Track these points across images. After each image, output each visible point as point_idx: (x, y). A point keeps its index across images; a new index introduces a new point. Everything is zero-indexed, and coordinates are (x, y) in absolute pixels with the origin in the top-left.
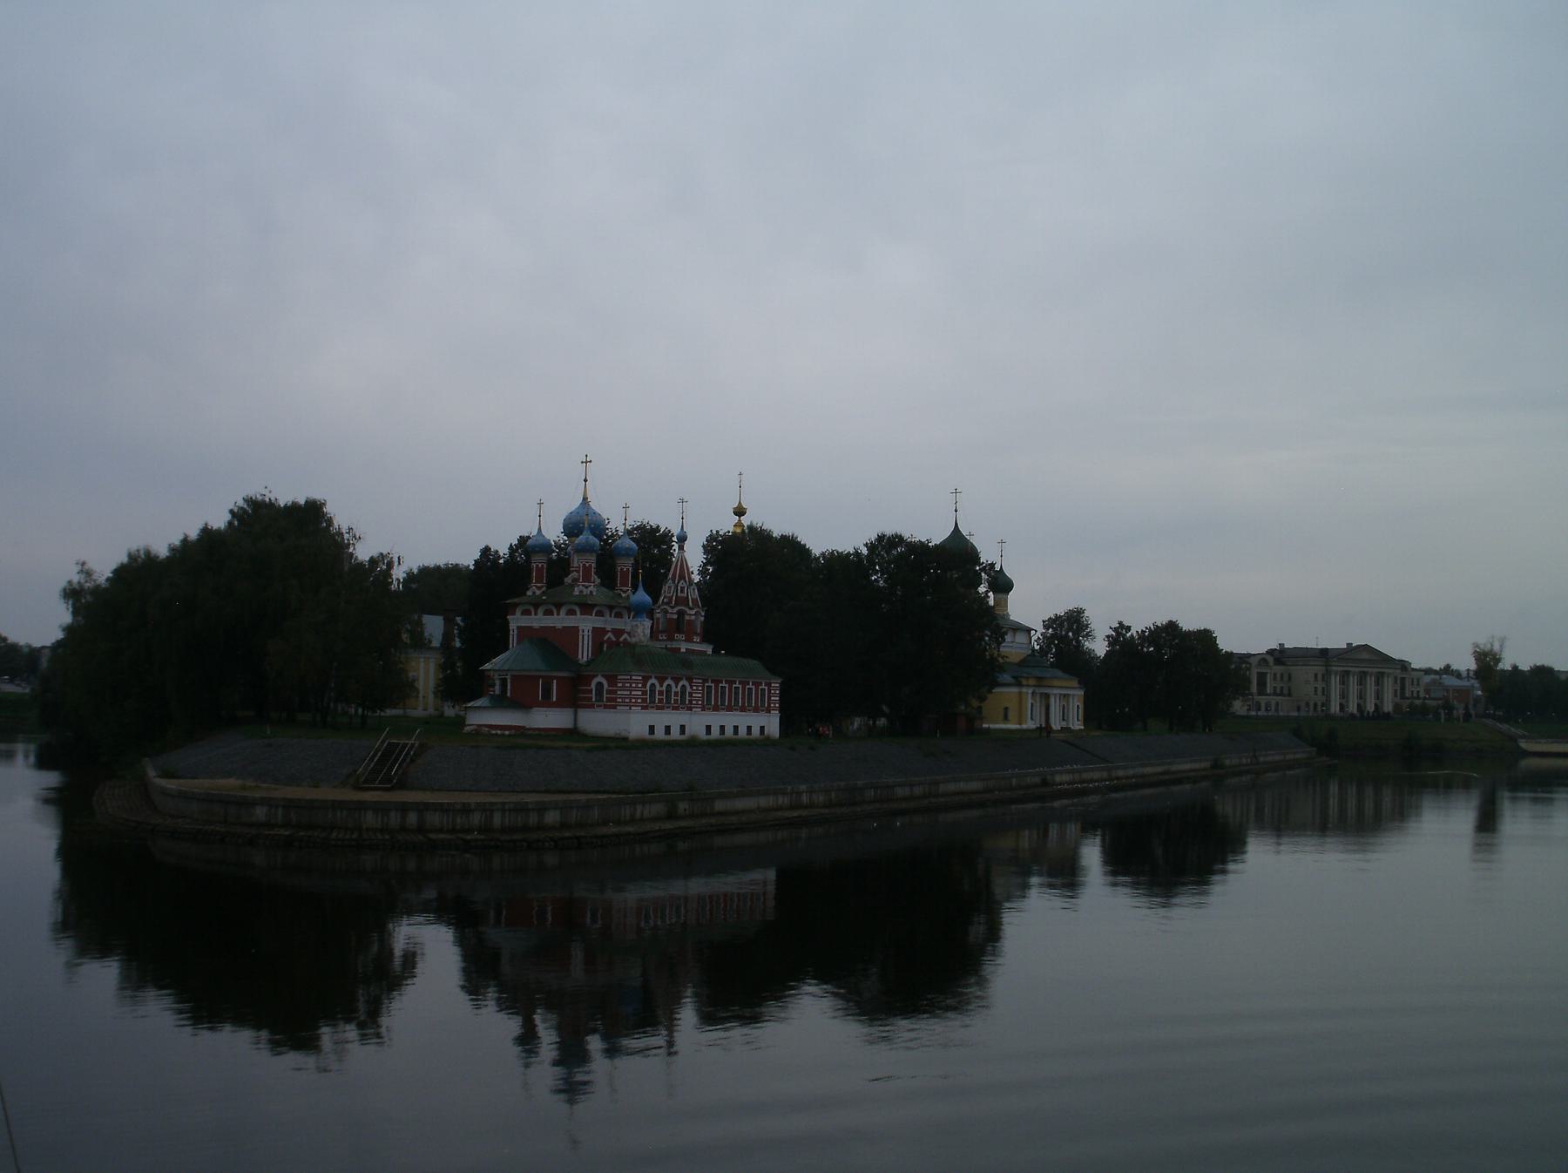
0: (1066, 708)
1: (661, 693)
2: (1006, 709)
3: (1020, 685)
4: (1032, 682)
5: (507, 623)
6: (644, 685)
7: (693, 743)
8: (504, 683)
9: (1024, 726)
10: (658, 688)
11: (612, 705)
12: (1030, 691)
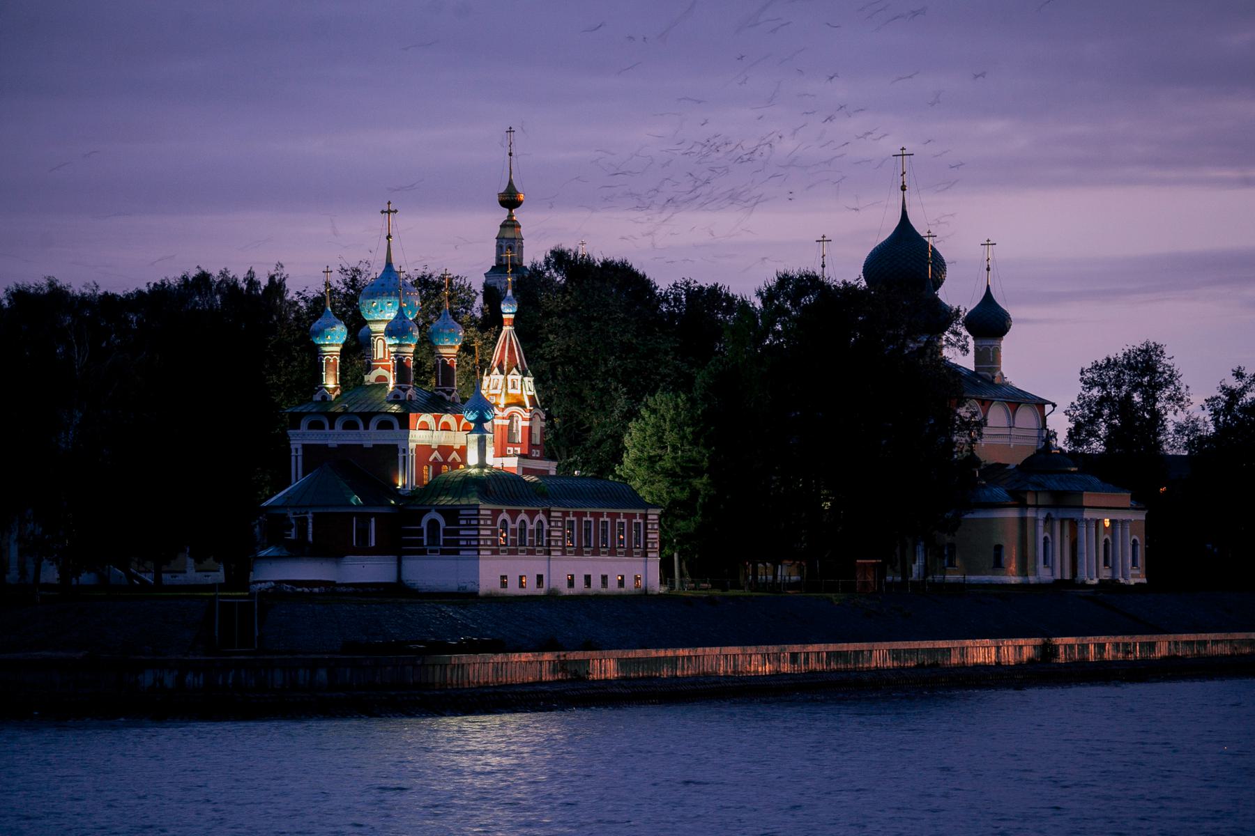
0: (1111, 538)
1: (532, 531)
2: (999, 548)
3: (1022, 505)
4: (1042, 499)
5: (286, 441)
6: (494, 523)
7: (553, 598)
8: (302, 522)
9: (1032, 579)
10: (529, 527)
11: (452, 549)
12: (1042, 515)
